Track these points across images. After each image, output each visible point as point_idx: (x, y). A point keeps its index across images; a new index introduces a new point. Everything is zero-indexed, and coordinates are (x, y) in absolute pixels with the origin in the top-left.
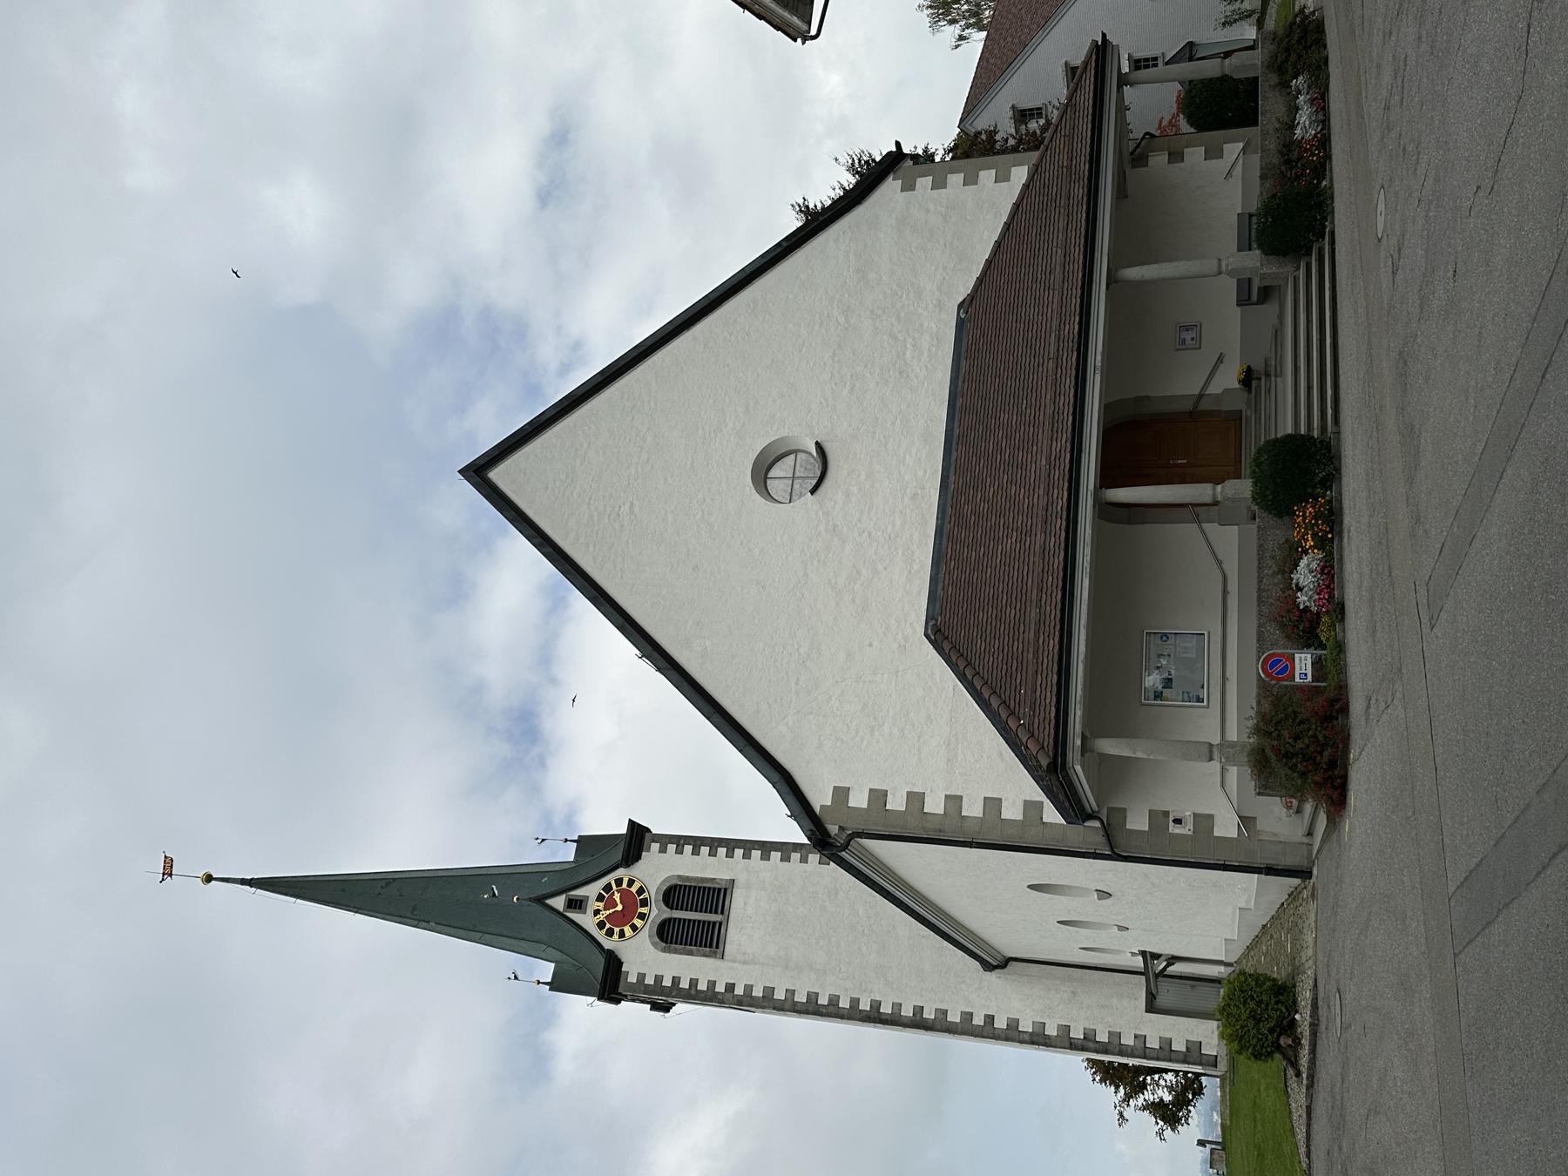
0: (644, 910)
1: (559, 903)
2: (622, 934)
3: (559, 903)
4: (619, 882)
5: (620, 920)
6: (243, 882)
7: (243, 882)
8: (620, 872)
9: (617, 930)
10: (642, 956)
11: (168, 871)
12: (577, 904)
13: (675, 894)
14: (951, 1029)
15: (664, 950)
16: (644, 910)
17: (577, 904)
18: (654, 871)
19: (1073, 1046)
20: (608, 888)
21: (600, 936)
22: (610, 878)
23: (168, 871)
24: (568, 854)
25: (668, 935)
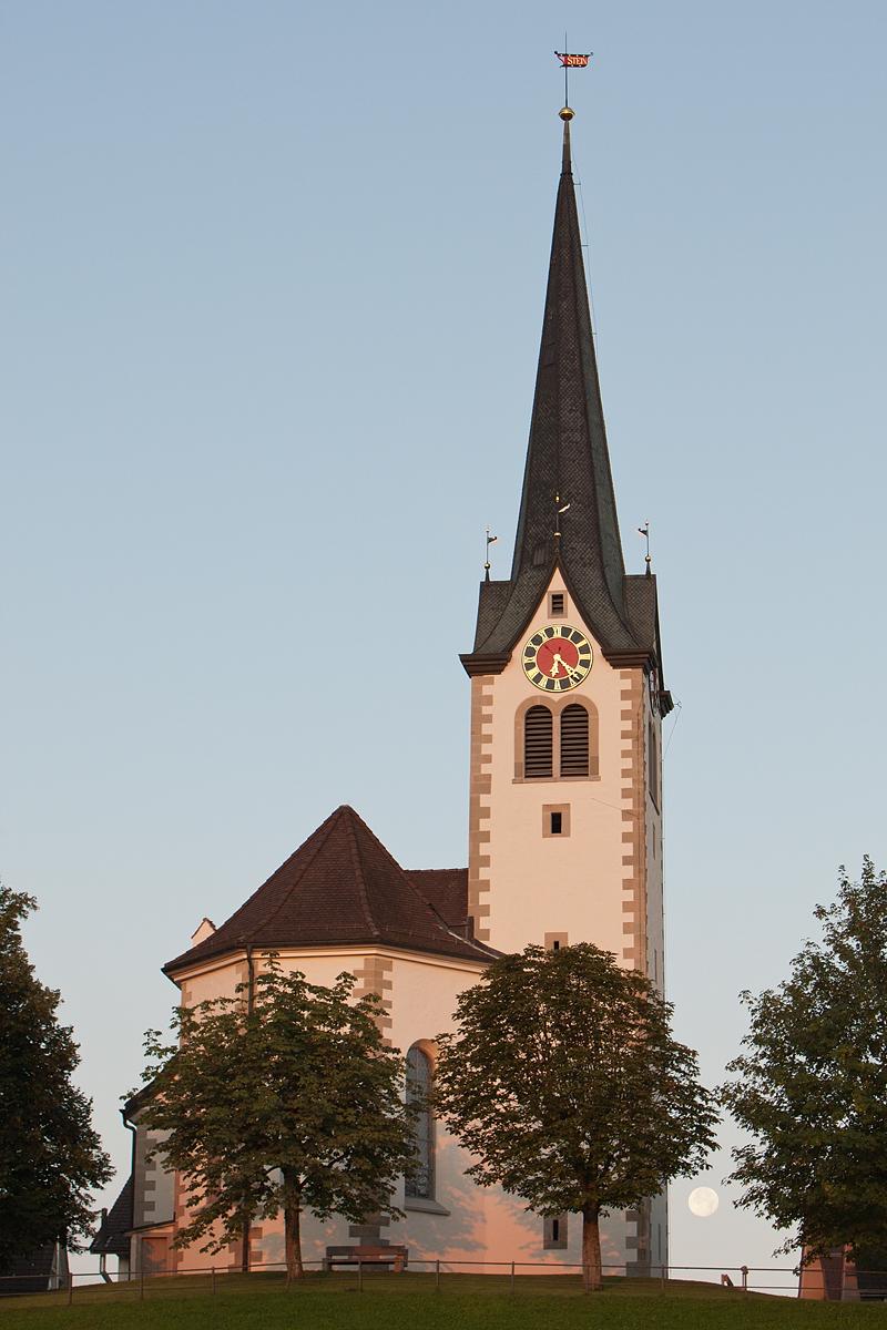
0: (557, 686)
1: (557, 584)
2: (529, 666)
3: (557, 584)
4: (585, 650)
5: (545, 651)
6: (567, 176)
7: (567, 176)
8: (596, 648)
9: (534, 659)
10: (515, 687)
11: (568, 61)
12: (557, 605)
13: (577, 715)
14: (475, 750)
15: (522, 705)
16: (557, 686)
17: (557, 605)
18: (606, 689)
19: (474, 849)
20: (577, 637)
21: (526, 641)
22: (589, 638)
23: (568, 61)
24: (634, 567)
25: (536, 716)
